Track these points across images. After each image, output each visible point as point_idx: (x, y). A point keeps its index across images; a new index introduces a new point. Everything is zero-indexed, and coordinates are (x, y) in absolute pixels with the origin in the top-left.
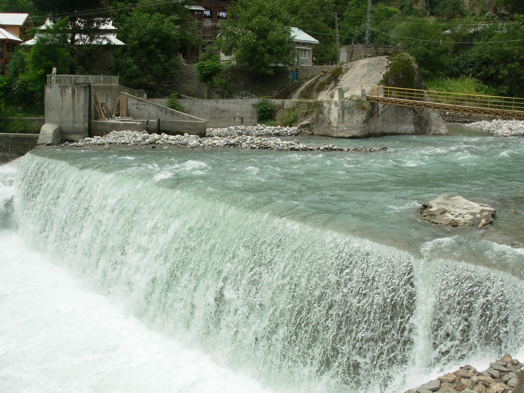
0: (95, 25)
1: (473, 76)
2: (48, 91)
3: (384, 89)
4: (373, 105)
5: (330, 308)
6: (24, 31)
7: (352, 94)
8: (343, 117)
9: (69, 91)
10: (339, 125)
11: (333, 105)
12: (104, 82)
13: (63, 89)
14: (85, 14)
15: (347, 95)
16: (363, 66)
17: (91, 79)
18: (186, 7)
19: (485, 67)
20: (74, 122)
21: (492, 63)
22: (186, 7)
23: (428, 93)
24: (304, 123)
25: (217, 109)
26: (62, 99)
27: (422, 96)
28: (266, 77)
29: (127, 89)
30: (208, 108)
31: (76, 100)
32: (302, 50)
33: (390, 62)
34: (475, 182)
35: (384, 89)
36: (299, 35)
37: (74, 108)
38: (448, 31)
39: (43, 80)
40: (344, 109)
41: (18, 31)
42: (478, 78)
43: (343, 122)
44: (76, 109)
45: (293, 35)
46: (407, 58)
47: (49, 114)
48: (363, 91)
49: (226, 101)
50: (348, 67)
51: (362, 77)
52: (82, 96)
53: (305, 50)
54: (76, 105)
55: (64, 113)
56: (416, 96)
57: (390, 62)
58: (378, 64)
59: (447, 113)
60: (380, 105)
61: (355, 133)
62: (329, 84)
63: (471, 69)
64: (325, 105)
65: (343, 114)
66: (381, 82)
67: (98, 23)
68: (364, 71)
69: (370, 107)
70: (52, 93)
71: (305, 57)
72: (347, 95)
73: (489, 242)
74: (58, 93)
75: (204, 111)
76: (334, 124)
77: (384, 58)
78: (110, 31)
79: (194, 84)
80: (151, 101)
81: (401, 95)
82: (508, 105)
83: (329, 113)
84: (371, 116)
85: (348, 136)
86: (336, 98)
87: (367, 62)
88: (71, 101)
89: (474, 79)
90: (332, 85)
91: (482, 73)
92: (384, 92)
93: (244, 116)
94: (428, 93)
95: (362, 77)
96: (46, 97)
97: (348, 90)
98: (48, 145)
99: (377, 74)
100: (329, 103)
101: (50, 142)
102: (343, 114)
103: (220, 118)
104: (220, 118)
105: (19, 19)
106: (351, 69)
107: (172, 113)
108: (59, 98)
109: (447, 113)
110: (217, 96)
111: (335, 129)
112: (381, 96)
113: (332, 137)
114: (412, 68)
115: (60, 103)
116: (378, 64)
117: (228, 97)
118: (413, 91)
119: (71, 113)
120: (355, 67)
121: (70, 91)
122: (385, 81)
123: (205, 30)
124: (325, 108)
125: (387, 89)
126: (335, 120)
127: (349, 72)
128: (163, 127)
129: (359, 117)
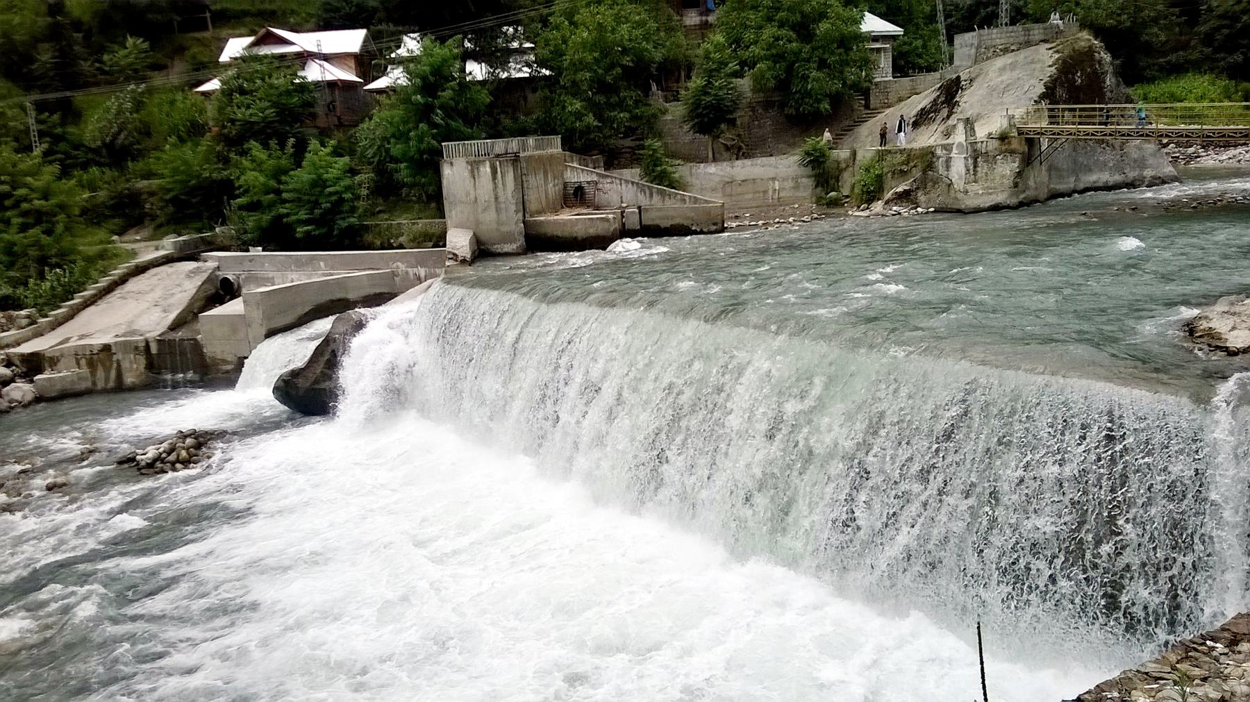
2: (447, 171)
3: (1050, 110)
4: (1031, 142)
6: (368, 63)
9: (486, 169)
10: (968, 187)
11: (955, 151)
12: (537, 147)
13: (474, 166)
15: (981, 132)
16: (1002, 70)
17: (514, 144)
24: (900, 189)
26: (471, 182)
28: (807, 100)
29: (576, 157)
31: (500, 185)
36: (873, 24)
37: (496, 198)
40: (976, 155)
41: (352, 64)
43: (975, 182)
44: (502, 199)
47: (453, 213)
49: (748, 162)
50: (973, 76)
51: (1004, 85)
52: (510, 177)
53: (878, 50)
54: (501, 193)
57: (1057, 56)
60: (1045, 144)
61: (1001, 198)
62: (937, 111)
64: (939, 152)
66: (1043, 97)
69: (1024, 146)
70: (455, 174)
72: (981, 132)
74: (467, 174)
76: (958, 184)
79: (685, 136)
80: (616, 173)
81: (1086, 119)
83: (948, 168)
84: (1028, 164)
86: (959, 137)
87: (1010, 61)
88: (490, 186)
90: (945, 112)
95: (1004, 85)
96: (445, 183)
99: (1032, 81)
100: (948, 148)
105: (351, 40)
106: (980, 79)
107: (661, 192)
108: (469, 182)
110: (726, 155)
111: (960, 196)
112: (1044, 124)
113: (959, 211)
114: (1100, 62)
115: (472, 192)
117: (747, 156)
118: (1094, 109)
120: (987, 74)
121: (488, 170)
122: (1049, 94)
123: (689, 30)
126: (960, 178)
127: (975, 84)
129: (1007, 168)
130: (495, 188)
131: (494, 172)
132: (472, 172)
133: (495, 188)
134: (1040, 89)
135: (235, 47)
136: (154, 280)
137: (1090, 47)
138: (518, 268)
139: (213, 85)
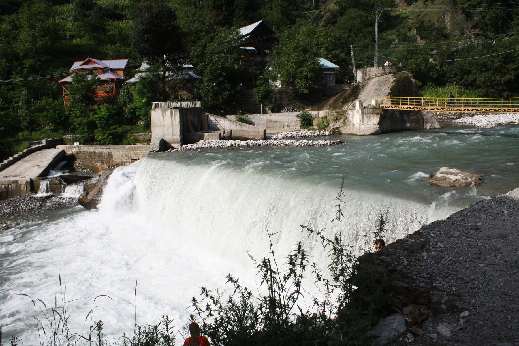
0: (179, 65)
1: (457, 83)
3: (391, 98)
5: (102, 235)
6: (129, 71)
7: (369, 104)
8: (363, 121)
10: (360, 127)
14: (171, 58)
18: (242, 48)
19: (466, 76)
20: (173, 135)
21: (471, 73)
22: (242, 48)
23: (424, 99)
25: (271, 121)
26: (165, 122)
27: (420, 102)
30: (265, 121)
32: (327, 74)
33: (394, 79)
34: (297, 143)
35: (391, 98)
38: (435, 52)
39: (148, 107)
42: (461, 85)
44: (174, 125)
45: (321, 63)
46: (406, 75)
48: (376, 101)
49: (277, 114)
53: (330, 74)
55: (166, 129)
56: (416, 102)
57: (394, 79)
58: (386, 80)
59: (438, 113)
63: (455, 79)
65: (363, 119)
66: (389, 94)
67: (181, 64)
68: (375, 87)
71: (330, 79)
73: (463, 209)
74: (161, 115)
75: (262, 122)
76: (357, 126)
77: (390, 76)
78: (190, 69)
82: (486, 103)
85: (368, 134)
88: (170, 120)
89: (457, 86)
91: (463, 81)
92: (392, 101)
93: (290, 124)
94: (424, 99)
96: (152, 118)
97: (365, 100)
98: (157, 151)
101: (158, 149)
102: (363, 119)
103: (273, 127)
104: (273, 127)
105: (122, 63)
109: (438, 113)
115: (163, 122)
116: (386, 80)
118: (413, 99)
119: (171, 128)
124: (349, 115)
125: (393, 99)
128: (234, 134)
130: (172, 121)
131: (172, 114)
132: (163, 114)
133: (172, 121)
134: (389, 91)
135: (77, 65)
136: (18, 165)
137: (408, 76)
138: (104, 70)
139: (69, 79)
